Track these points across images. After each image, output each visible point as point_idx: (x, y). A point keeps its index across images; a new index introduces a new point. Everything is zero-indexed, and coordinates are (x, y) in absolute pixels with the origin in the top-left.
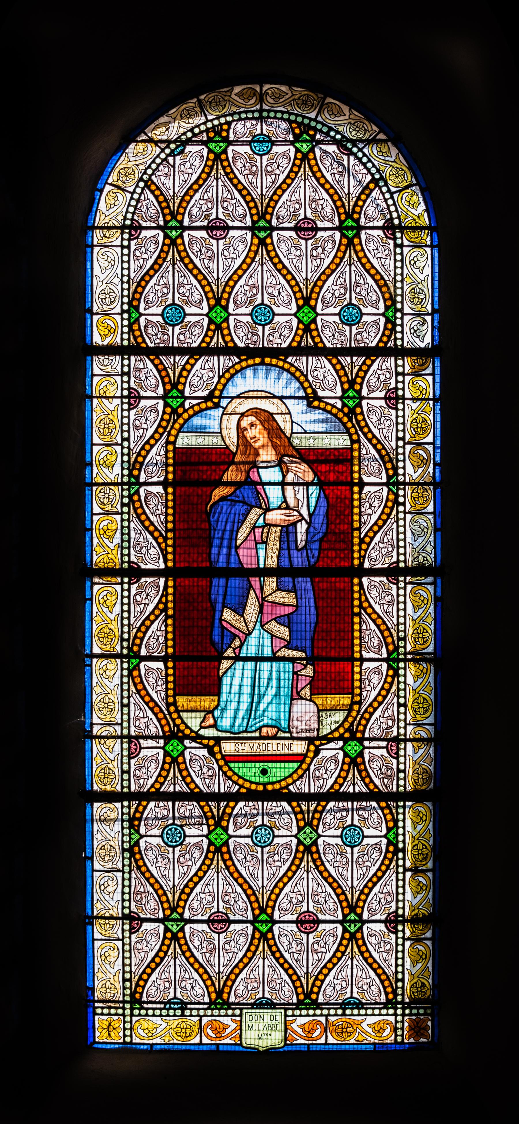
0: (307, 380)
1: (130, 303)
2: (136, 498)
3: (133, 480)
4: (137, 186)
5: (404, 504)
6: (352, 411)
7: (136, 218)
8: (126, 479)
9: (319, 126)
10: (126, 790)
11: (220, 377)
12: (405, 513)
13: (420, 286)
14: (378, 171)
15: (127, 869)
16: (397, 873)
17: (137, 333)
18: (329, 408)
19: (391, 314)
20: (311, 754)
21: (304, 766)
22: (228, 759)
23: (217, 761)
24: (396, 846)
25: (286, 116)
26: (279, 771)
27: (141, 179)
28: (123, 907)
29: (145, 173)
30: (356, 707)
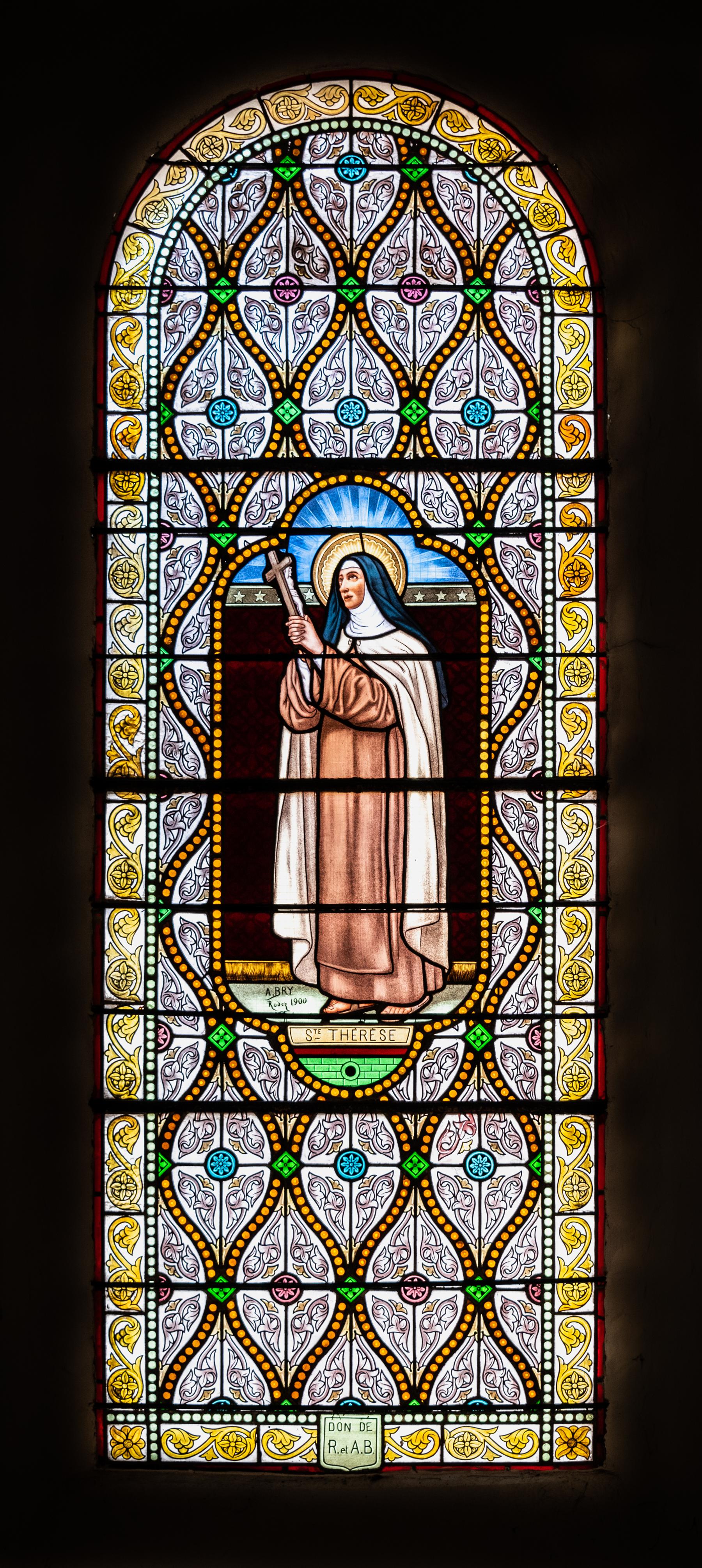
0: (415, 508)
1: (160, 397)
2: (168, 676)
3: (163, 651)
4: (171, 228)
5: (553, 687)
6: (480, 551)
7: (168, 274)
8: (153, 649)
9: (434, 143)
10: (151, 1097)
11: (289, 504)
12: (554, 699)
13: (219, 1439)
14: (518, 209)
15: (151, 1211)
16: (544, 1217)
17: (171, 440)
18: (446, 548)
19: (536, 411)
20: (417, 1045)
21: (408, 1063)
22: (301, 1052)
23: (283, 1055)
24: (541, 1179)
25: (387, 128)
26: (370, 1071)
27: (177, 218)
28: (147, 1267)
29: (183, 208)
30: (482, 978)
